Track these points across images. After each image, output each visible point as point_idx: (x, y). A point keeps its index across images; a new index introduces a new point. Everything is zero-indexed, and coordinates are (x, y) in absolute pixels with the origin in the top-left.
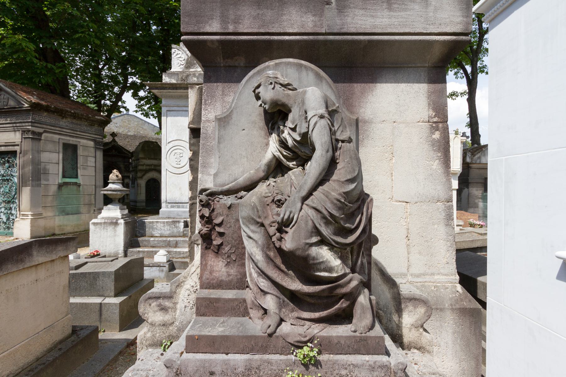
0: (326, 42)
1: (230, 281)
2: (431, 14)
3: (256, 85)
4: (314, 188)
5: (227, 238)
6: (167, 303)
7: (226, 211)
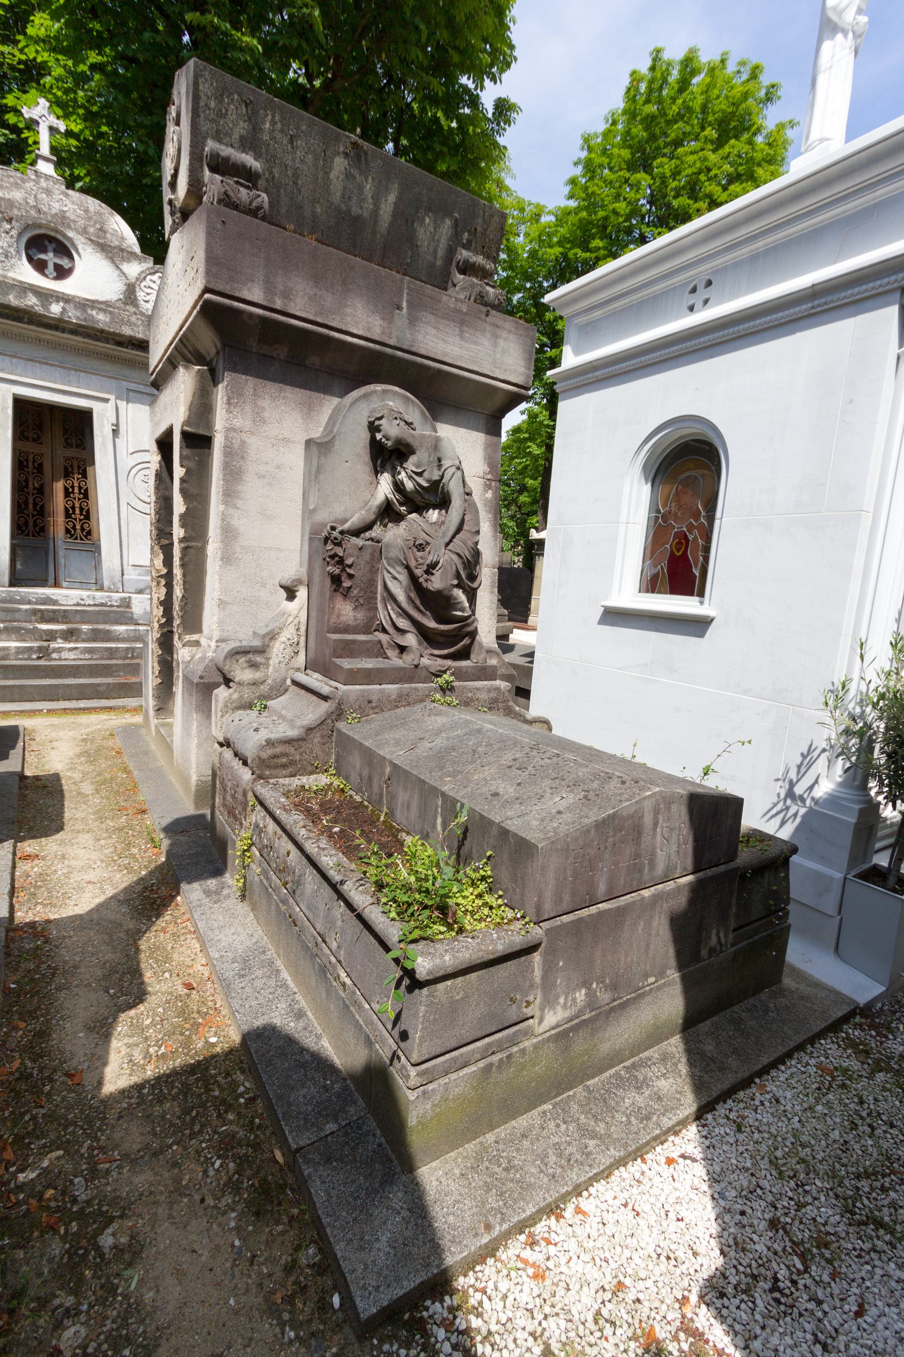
0: (393, 358)
1: (357, 626)
2: (498, 356)
3: (379, 415)
4: (453, 537)
5: (356, 580)
6: (259, 659)
7: (356, 552)
